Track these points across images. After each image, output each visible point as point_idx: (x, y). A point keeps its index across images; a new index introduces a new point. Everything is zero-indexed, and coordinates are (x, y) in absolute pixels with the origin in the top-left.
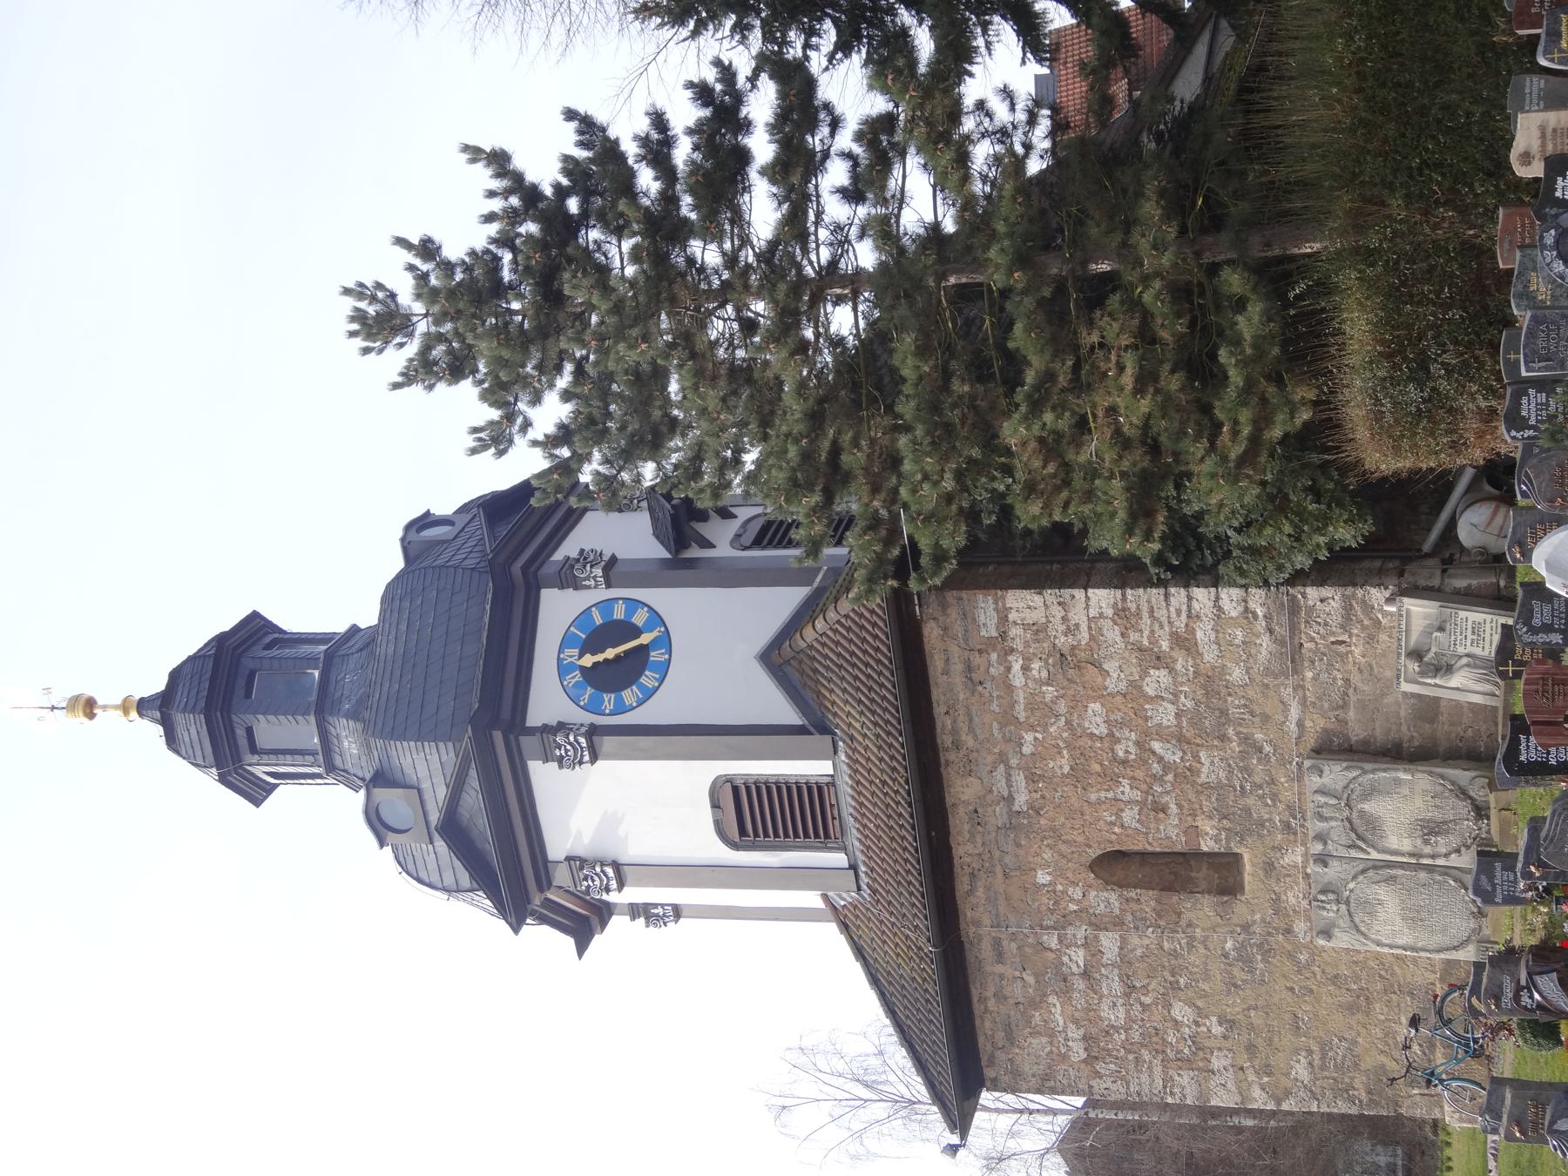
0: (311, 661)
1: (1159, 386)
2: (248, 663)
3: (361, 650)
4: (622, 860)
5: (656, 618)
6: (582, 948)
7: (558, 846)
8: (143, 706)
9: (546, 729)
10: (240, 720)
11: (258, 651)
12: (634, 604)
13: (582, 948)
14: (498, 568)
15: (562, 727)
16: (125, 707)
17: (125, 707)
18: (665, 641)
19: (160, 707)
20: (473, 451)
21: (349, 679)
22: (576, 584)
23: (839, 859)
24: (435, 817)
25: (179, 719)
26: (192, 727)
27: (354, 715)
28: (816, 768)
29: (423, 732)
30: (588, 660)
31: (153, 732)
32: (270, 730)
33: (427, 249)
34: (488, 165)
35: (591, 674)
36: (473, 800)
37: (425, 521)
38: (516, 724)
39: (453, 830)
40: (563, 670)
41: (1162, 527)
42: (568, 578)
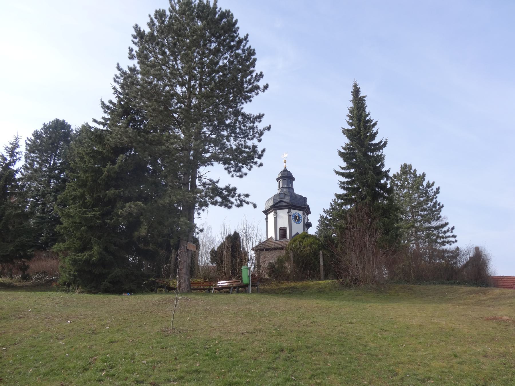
1: (296, 348)
3: (364, 268)
4: (277, 218)
6: (263, 212)
8: (285, 168)
12: (301, 220)
13: (263, 212)
16: (285, 166)
17: (285, 166)
19: (285, 170)
20: (320, 215)
23: (278, 239)
28: (288, 238)
30: (297, 216)
31: (283, 170)
34: (354, 90)
35: (296, 216)
36: (284, 204)
39: (281, 201)
40: (296, 213)
41: (375, 175)
42: (303, 214)
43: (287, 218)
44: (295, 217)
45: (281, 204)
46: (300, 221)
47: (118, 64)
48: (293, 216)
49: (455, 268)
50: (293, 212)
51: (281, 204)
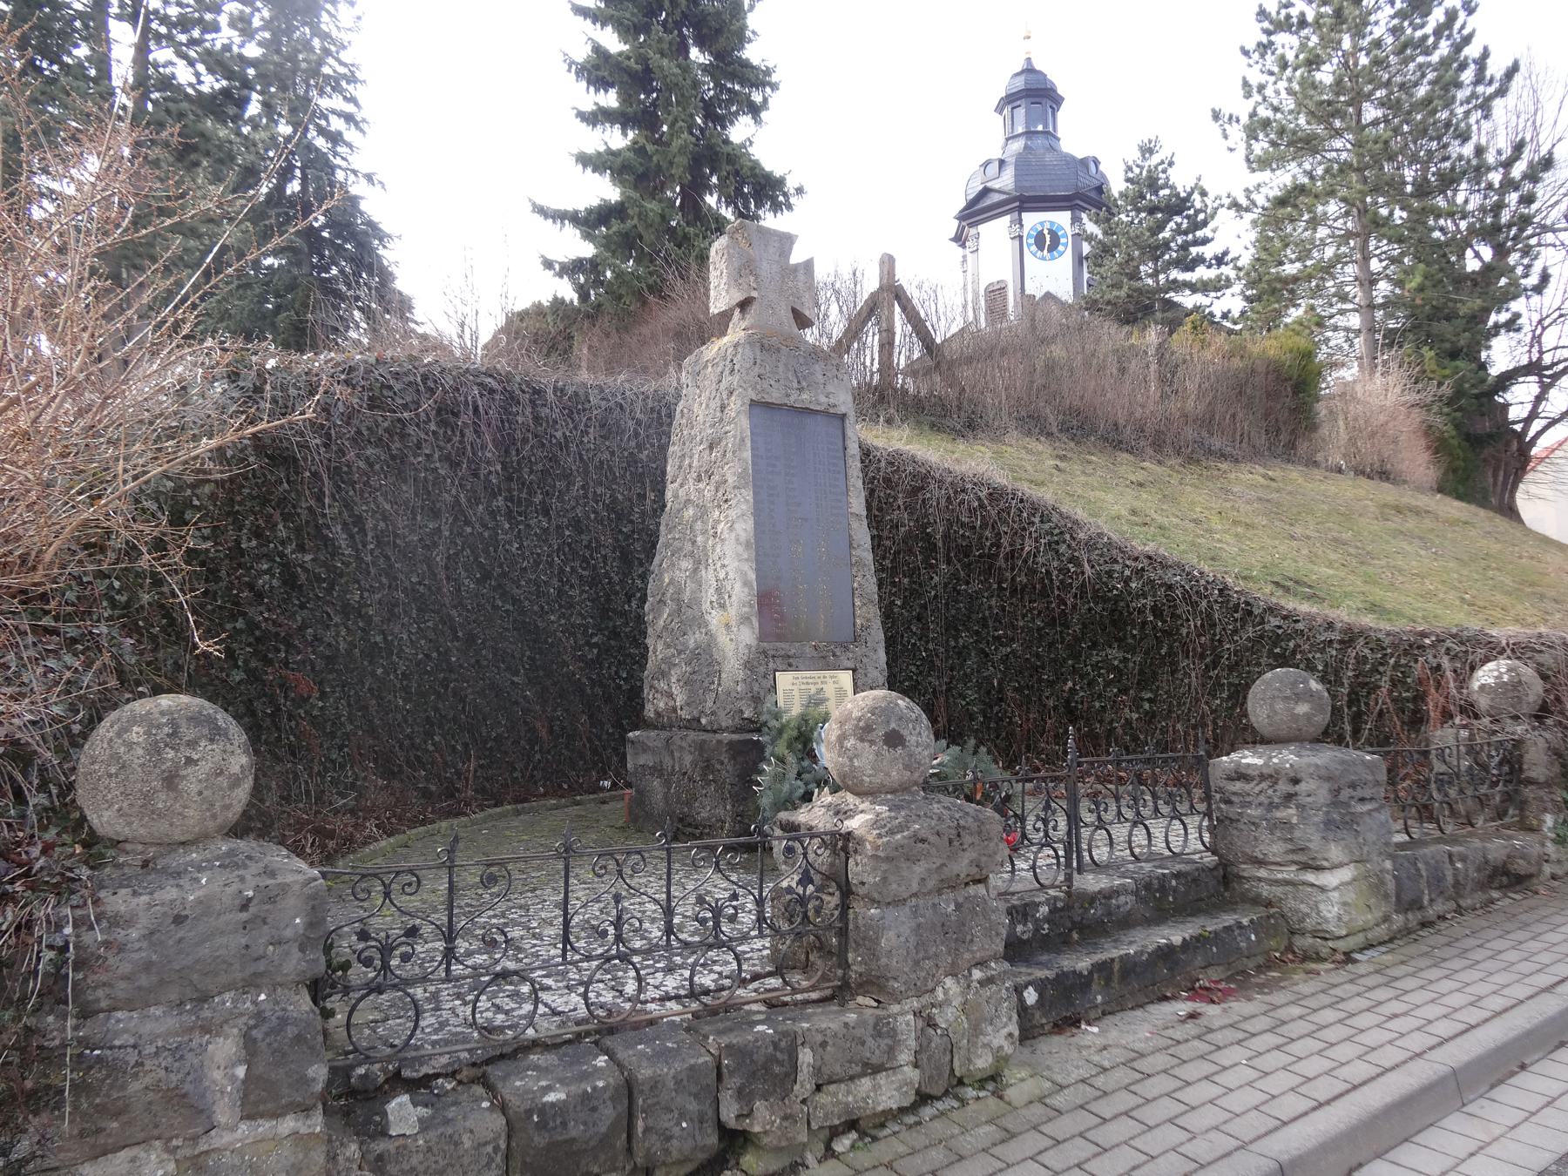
0: (1046, 126)
2: (1044, 101)
5: (1061, 254)
7: (982, 228)
9: (1021, 220)
10: (1022, 102)
11: (1049, 103)
12: (1066, 245)
14: (1078, 195)
15: (1022, 226)
18: (1043, 258)
19: (1029, 70)
21: (1039, 142)
22: (1073, 224)
24: (989, 185)
25: (1022, 78)
26: (1020, 83)
27: (1026, 147)
29: (1018, 176)
32: (1021, 113)
33: (1171, 164)
36: (996, 198)
37: (1096, 162)
38: (1021, 209)
39: (986, 191)
40: (1042, 223)
42: (1076, 220)
43: (1008, 248)
44: (1039, 240)
45: (988, 202)
46: (1061, 248)
47: (542, 211)
48: (1029, 236)
49: (1415, 282)
50: (1032, 220)
51: (988, 202)
